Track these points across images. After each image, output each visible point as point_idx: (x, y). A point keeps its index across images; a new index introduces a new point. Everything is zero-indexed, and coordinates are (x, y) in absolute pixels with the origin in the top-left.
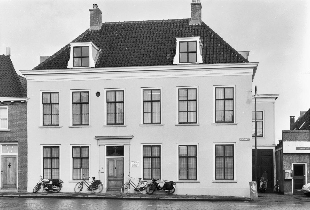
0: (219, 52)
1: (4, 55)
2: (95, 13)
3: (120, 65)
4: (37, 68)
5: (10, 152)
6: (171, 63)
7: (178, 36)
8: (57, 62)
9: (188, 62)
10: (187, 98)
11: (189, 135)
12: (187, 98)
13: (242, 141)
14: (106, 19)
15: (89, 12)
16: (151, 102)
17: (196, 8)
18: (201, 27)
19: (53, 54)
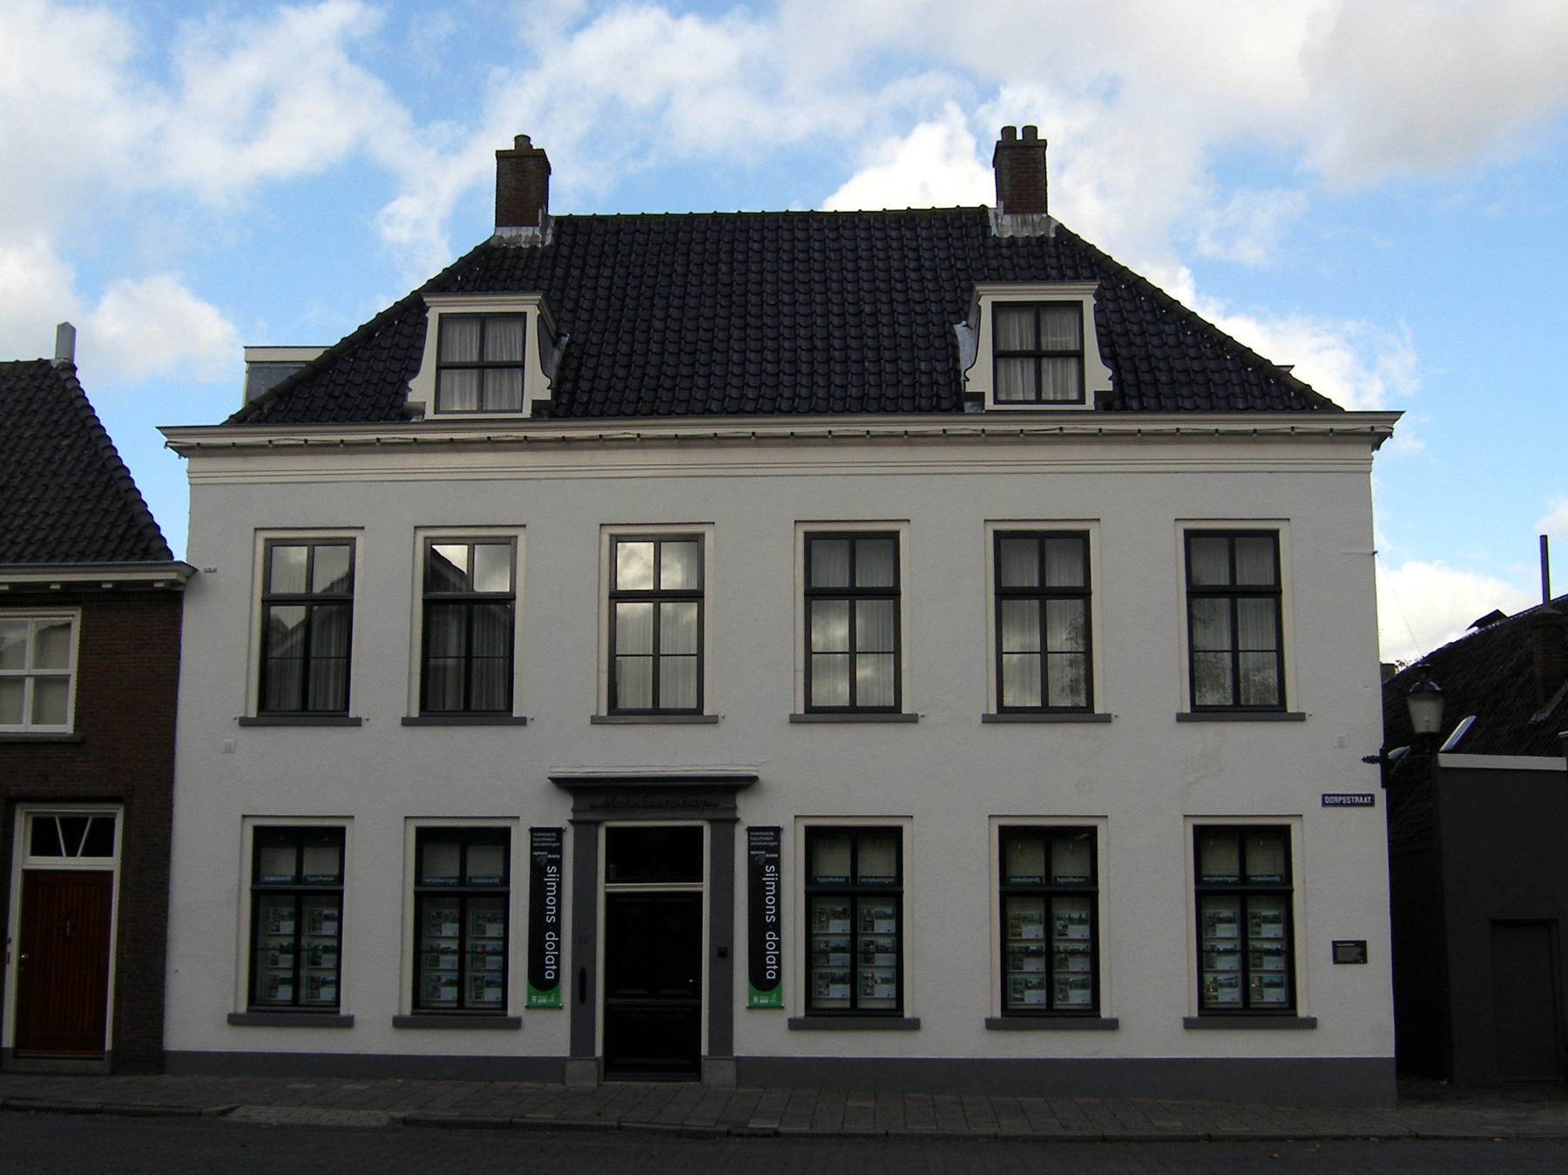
0: (1177, 369)
1: (41, 363)
2: (523, 171)
3: (682, 408)
4: (237, 420)
5: (74, 855)
6: (506, 601)
7: (987, 279)
8: (333, 392)
9: (1039, 401)
10: (1041, 573)
11: (1048, 776)
12: (1041, 573)
13: (1335, 805)
14: (568, 195)
15: (492, 164)
16: (662, 706)
17: (1020, 159)
18: (1056, 246)
19: (320, 352)
